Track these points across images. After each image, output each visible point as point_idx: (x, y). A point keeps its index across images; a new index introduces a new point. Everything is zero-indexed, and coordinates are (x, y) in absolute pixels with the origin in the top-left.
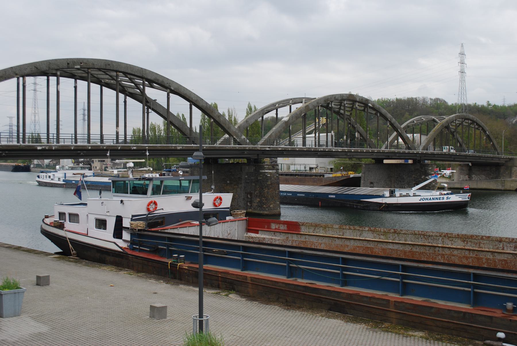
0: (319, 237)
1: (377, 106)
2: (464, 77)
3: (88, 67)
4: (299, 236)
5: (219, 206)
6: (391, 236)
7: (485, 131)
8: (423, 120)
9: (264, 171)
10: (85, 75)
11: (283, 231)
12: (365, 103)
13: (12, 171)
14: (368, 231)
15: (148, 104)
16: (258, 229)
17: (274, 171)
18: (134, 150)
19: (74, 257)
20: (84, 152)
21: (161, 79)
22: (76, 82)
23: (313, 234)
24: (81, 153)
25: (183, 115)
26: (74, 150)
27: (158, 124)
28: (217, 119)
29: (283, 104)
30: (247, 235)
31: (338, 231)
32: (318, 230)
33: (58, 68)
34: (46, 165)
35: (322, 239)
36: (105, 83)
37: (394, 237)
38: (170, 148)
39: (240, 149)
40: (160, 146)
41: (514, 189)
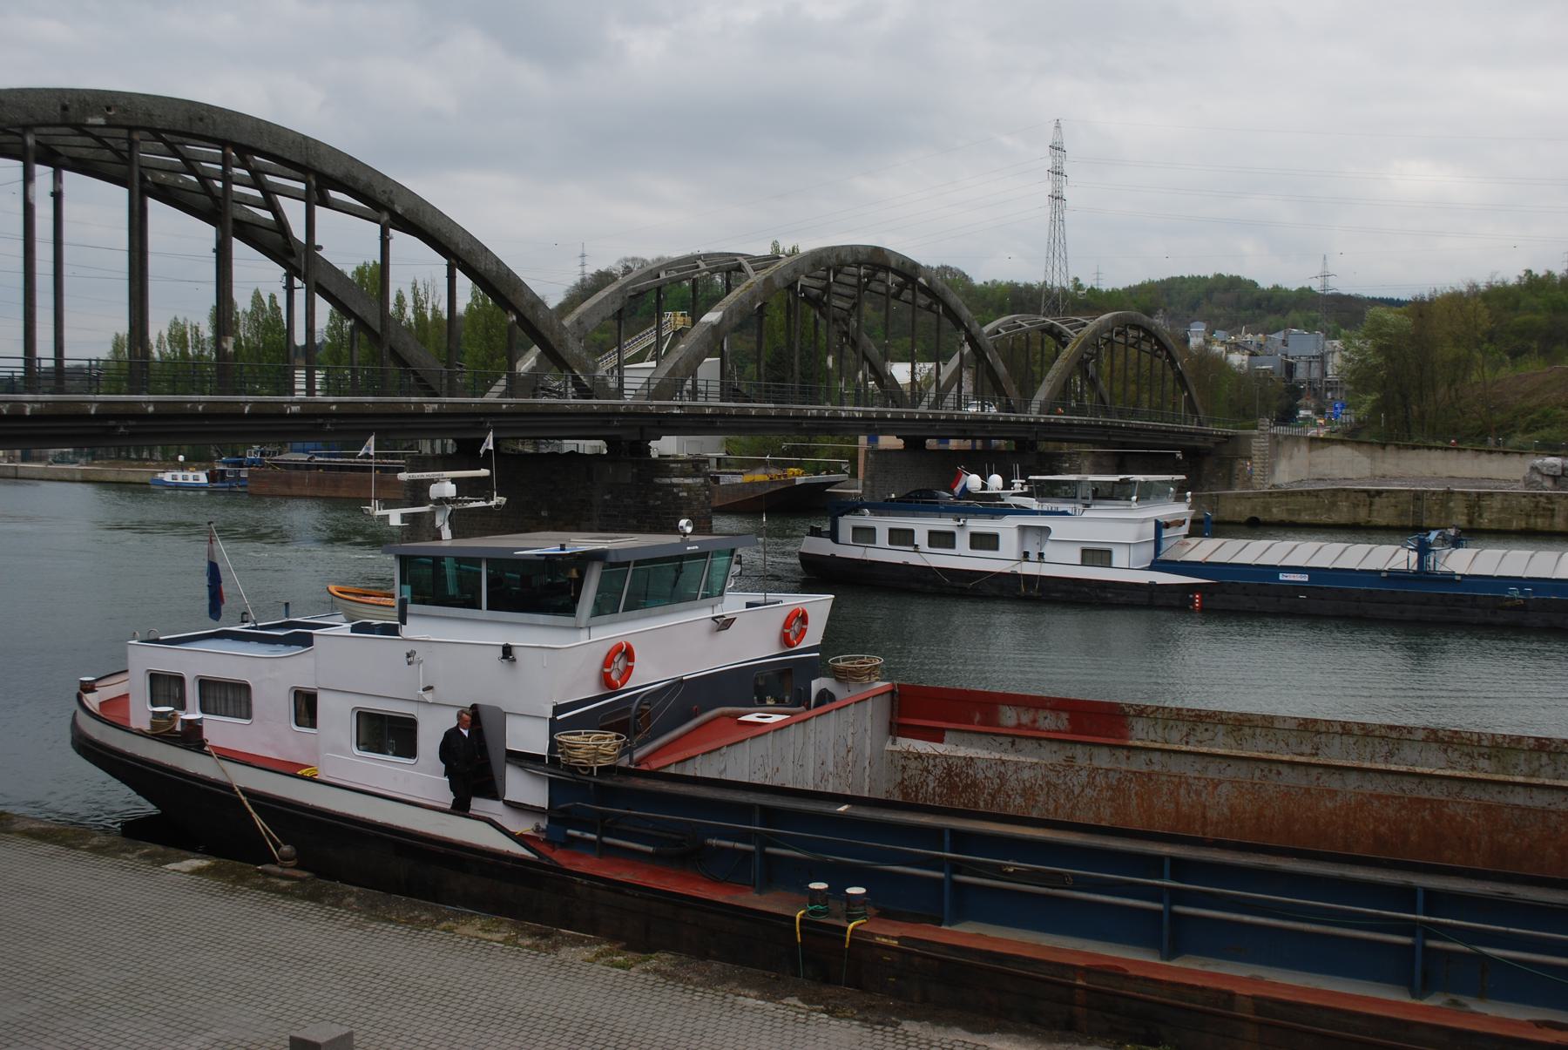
0: (1208, 759)
1: (939, 284)
2: (1062, 211)
3: (132, 123)
4: (1122, 754)
6: (1522, 762)
7: (1173, 362)
8: (1020, 326)
9: (667, 481)
11: (1052, 736)
12: (908, 272)
14: (1423, 740)
16: (944, 725)
17: (700, 480)
18: (293, 415)
19: (287, 871)
20: (131, 423)
22: (57, 179)
23: (1184, 748)
24: (118, 427)
25: (275, 298)
27: (195, 323)
28: (528, 314)
29: (678, 271)
30: (897, 748)
31: (1292, 740)
32: (1207, 735)
33: (31, 120)
35: (1224, 765)
36: (157, 185)
37: (1536, 764)
38: (405, 409)
39: (602, 411)
40: (373, 403)
41: (1244, 519)
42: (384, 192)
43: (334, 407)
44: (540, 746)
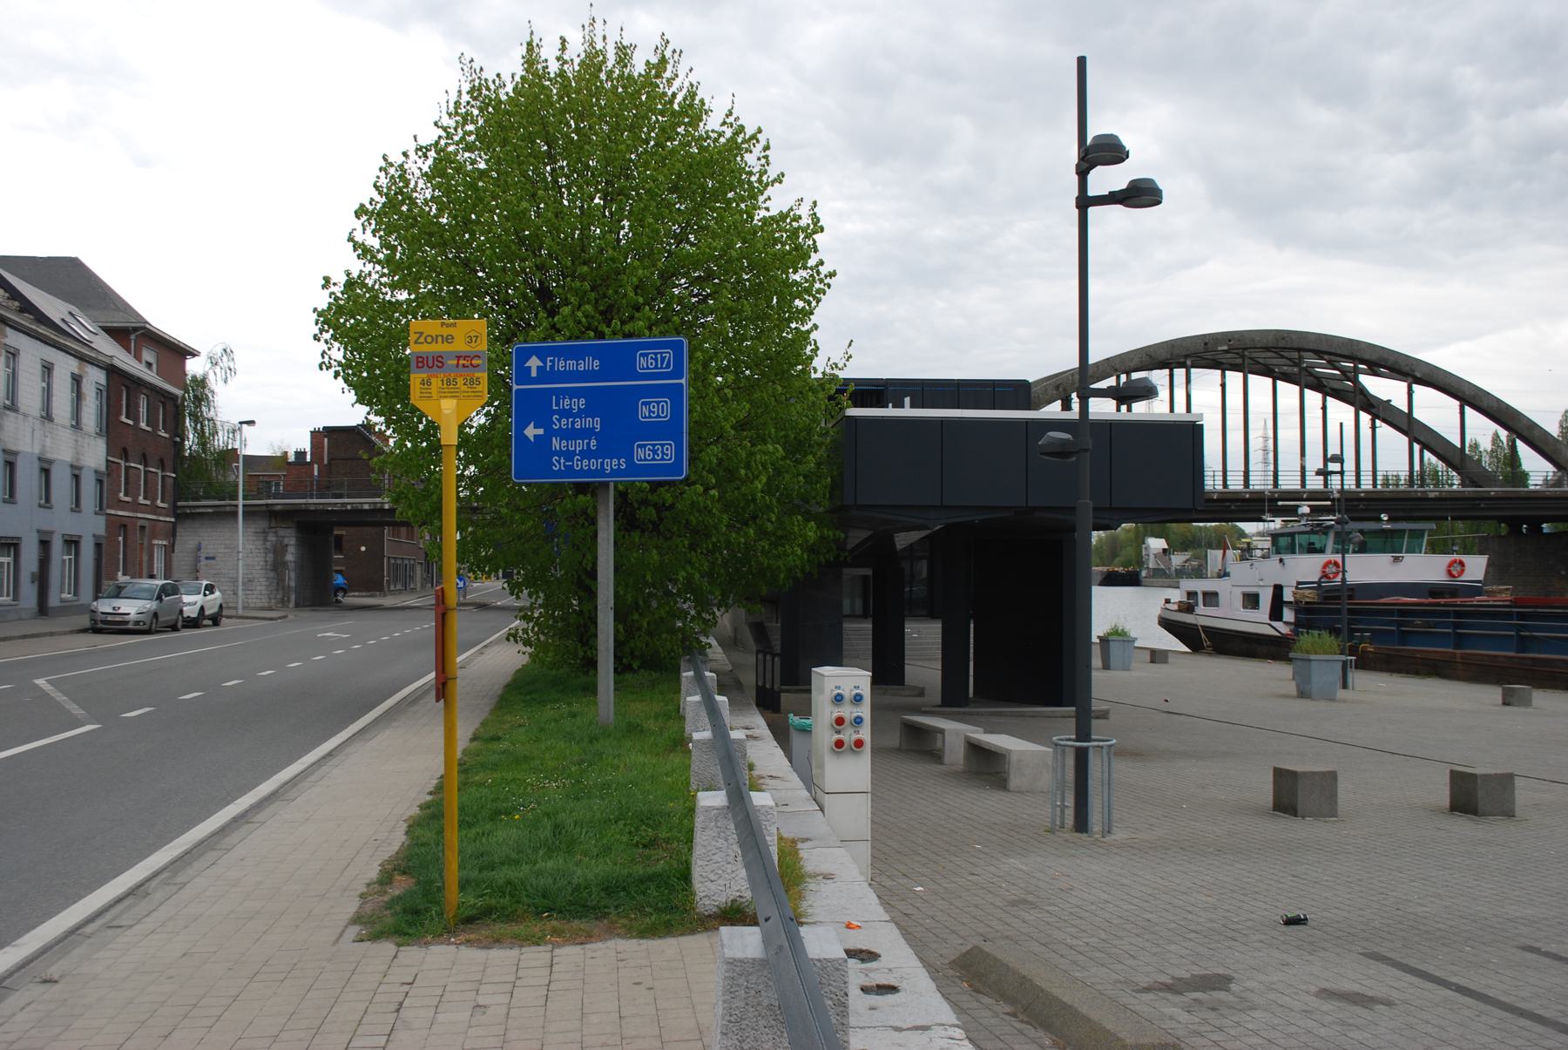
5: (1459, 576)
10: (1239, 361)
13: (1099, 585)
15: (1374, 411)
21: (1392, 359)
22: (1223, 376)
26: (1217, 500)
33: (1189, 352)
34: (1176, 570)
42: (1407, 365)
43: (1362, 495)
44: (1292, 599)
